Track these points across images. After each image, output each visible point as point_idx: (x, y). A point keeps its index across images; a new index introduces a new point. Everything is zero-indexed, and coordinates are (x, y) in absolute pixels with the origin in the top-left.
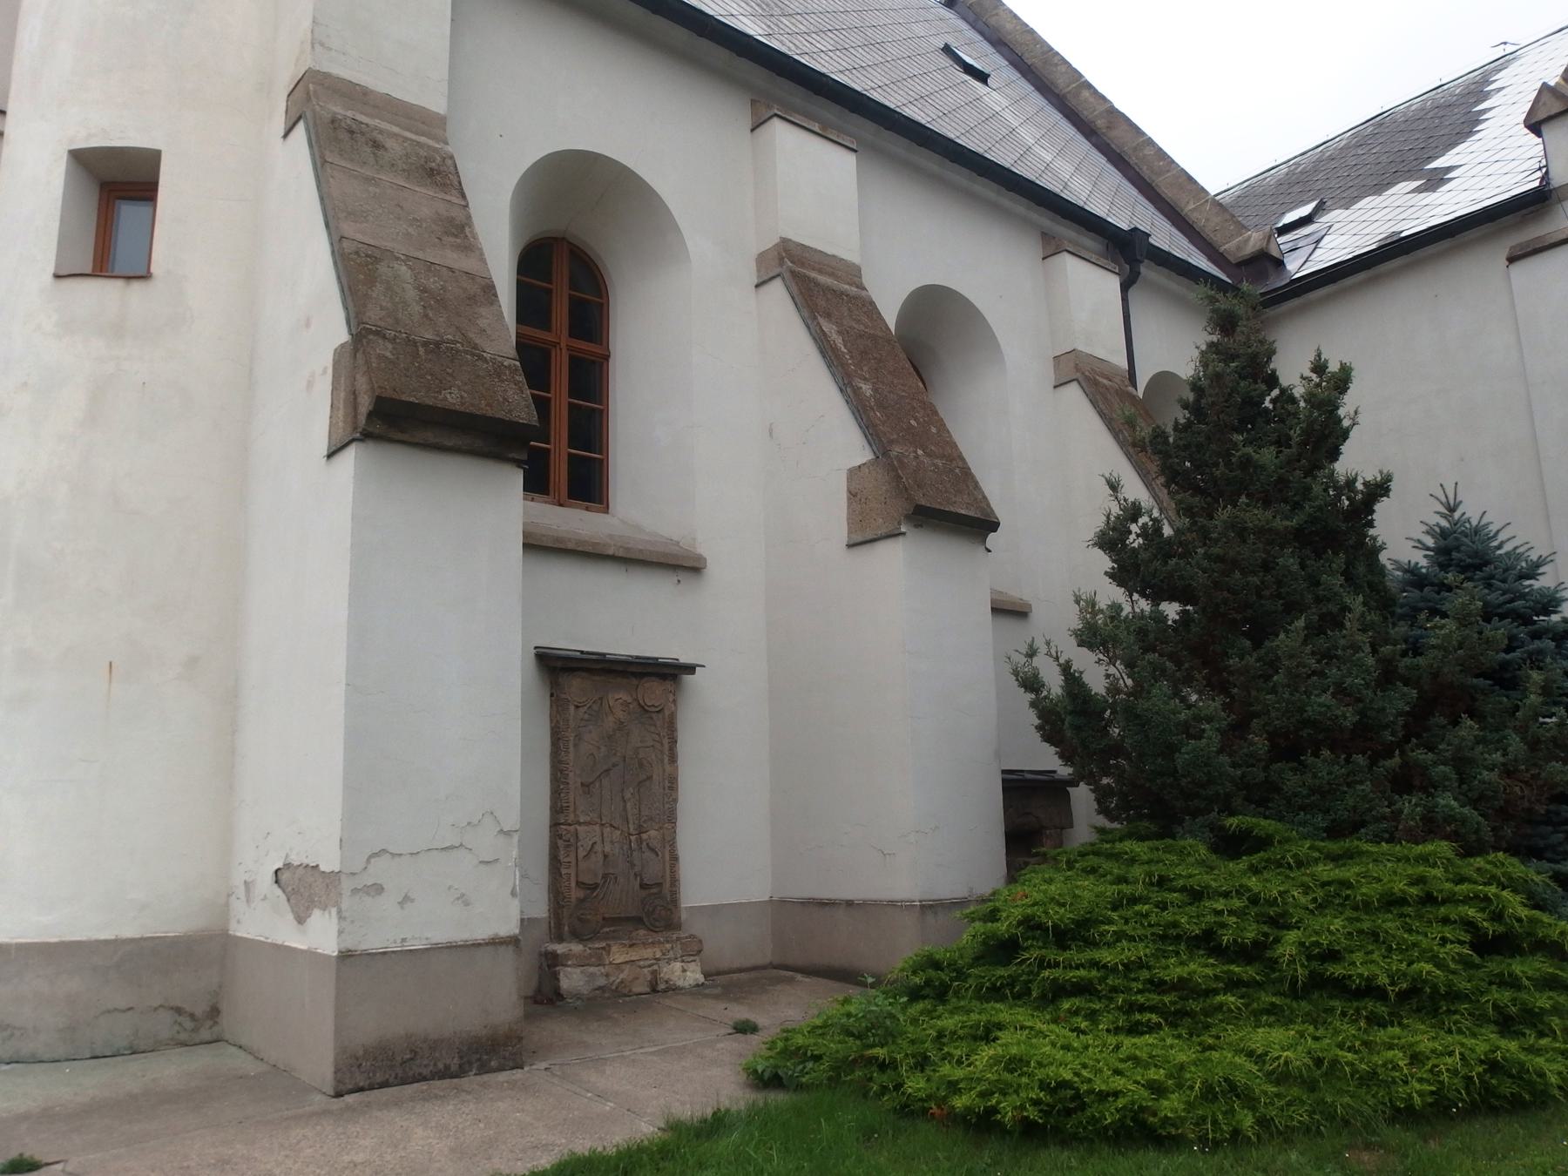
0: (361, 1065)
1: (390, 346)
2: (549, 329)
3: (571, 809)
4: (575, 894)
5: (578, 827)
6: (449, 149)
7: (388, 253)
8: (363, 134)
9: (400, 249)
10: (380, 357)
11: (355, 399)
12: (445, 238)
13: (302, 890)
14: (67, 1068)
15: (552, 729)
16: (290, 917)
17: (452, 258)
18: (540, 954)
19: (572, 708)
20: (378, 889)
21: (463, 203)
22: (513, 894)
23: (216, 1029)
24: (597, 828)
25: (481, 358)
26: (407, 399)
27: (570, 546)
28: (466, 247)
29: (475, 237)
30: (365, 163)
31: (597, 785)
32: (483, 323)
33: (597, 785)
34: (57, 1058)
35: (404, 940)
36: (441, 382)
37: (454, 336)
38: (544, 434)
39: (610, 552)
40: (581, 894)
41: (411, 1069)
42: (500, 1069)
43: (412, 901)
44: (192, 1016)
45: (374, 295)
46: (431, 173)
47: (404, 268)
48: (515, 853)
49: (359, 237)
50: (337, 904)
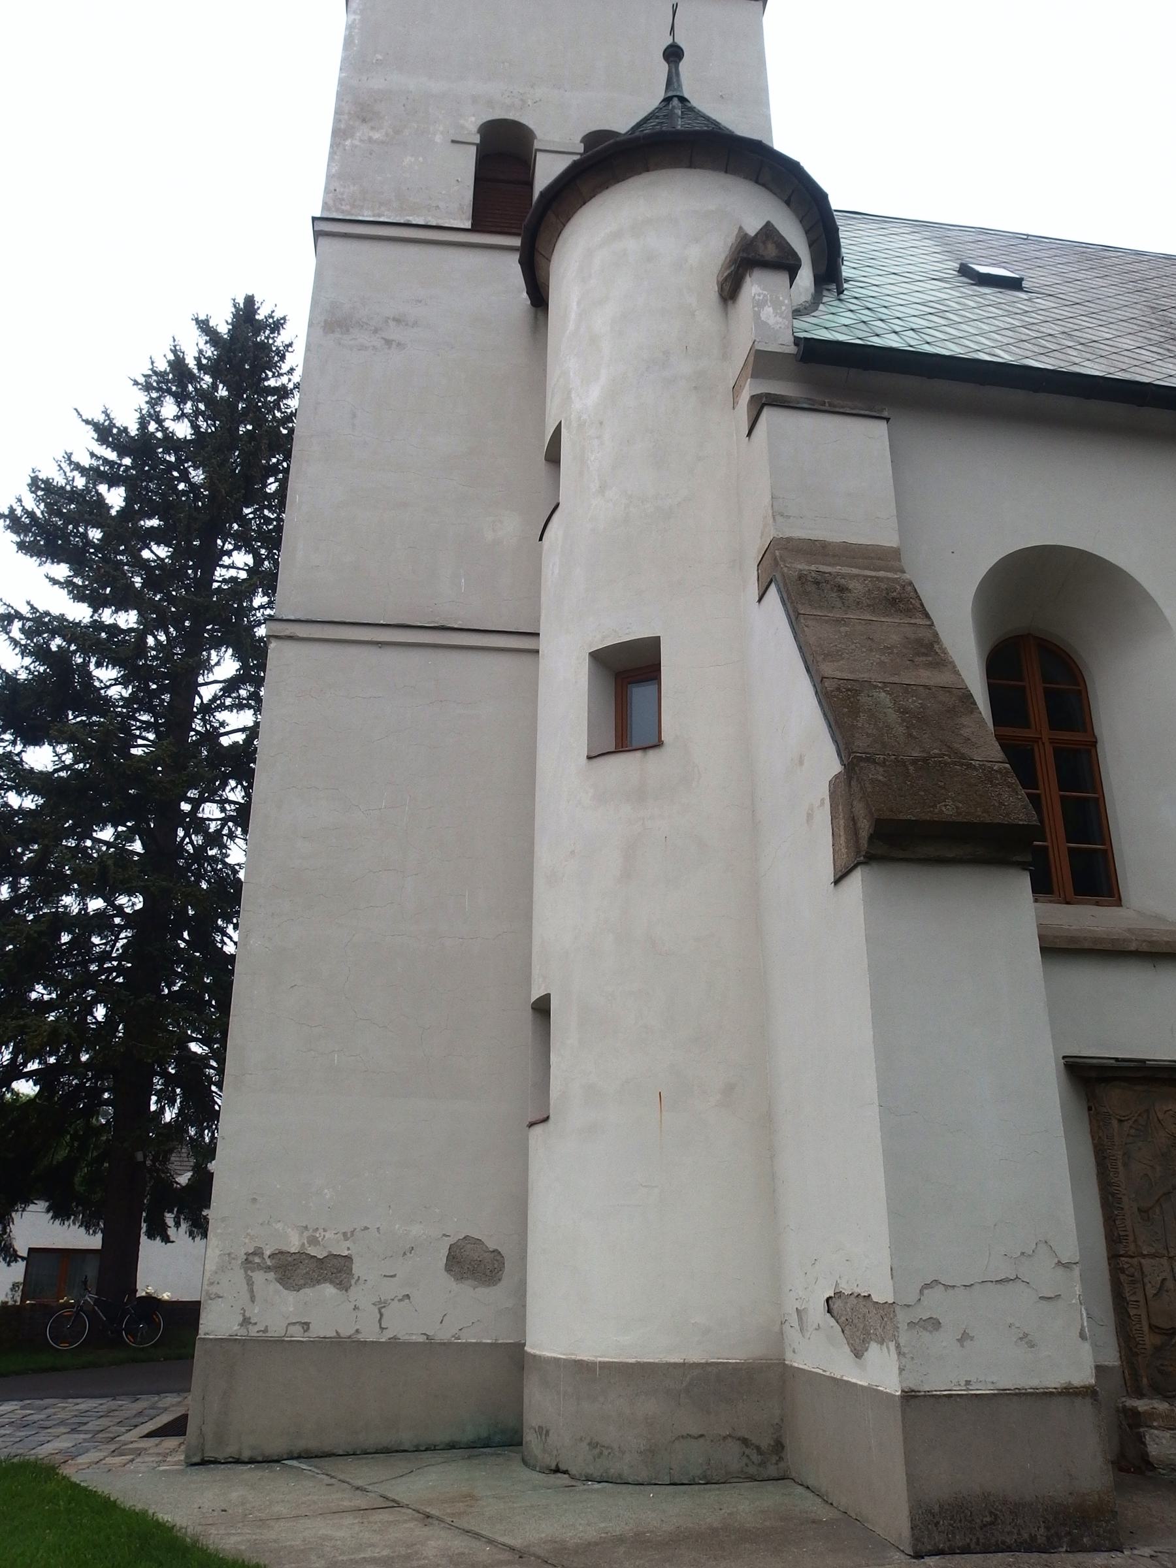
0: (938, 1523)
1: (881, 769)
2: (1027, 725)
3: (1131, 1238)
4: (1150, 1340)
5: (1143, 1261)
6: (907, 576)
7: (866, 684)
8: (827, 582)
9: (877, 677)
10: (872, 781)
11: (855, 824)
12: (917, 659)
13: (856, 1321)
14: (651, 1492)
15: (1095, 1146)
16: (847, 1349)
17: (926, 676)
18: (1118, 1411)
19: (1115, 1123)
20: (934, 1324)
21: (928, 623)
22: (1082, 1336)
23: (781, 1465)
24: (1164, 1261)
25: (970, 766)
26: (905, 817)
27: (1086, 945)
28: (938, 664)
29: (945, 652)
30: (833, 607)
31: (1157, 1210)
32: (966, 732)
33: (1157, 1210)
34: (641, 1482)
35: (968, 1383)
36: (935, 796)
37: (940, 750)
38: (1038, 831)
39: (1133, 947)
40: (1158, 1340)
41: (993, 1534)
42: (1096, 1549)
43: (972, 1338)
44: (758, 1448)
45: (860, 725)
46: (894, 602)
47: (883, 695)
48: (1078, 1289)
49: (839, 675)
50: (894, 1338)
